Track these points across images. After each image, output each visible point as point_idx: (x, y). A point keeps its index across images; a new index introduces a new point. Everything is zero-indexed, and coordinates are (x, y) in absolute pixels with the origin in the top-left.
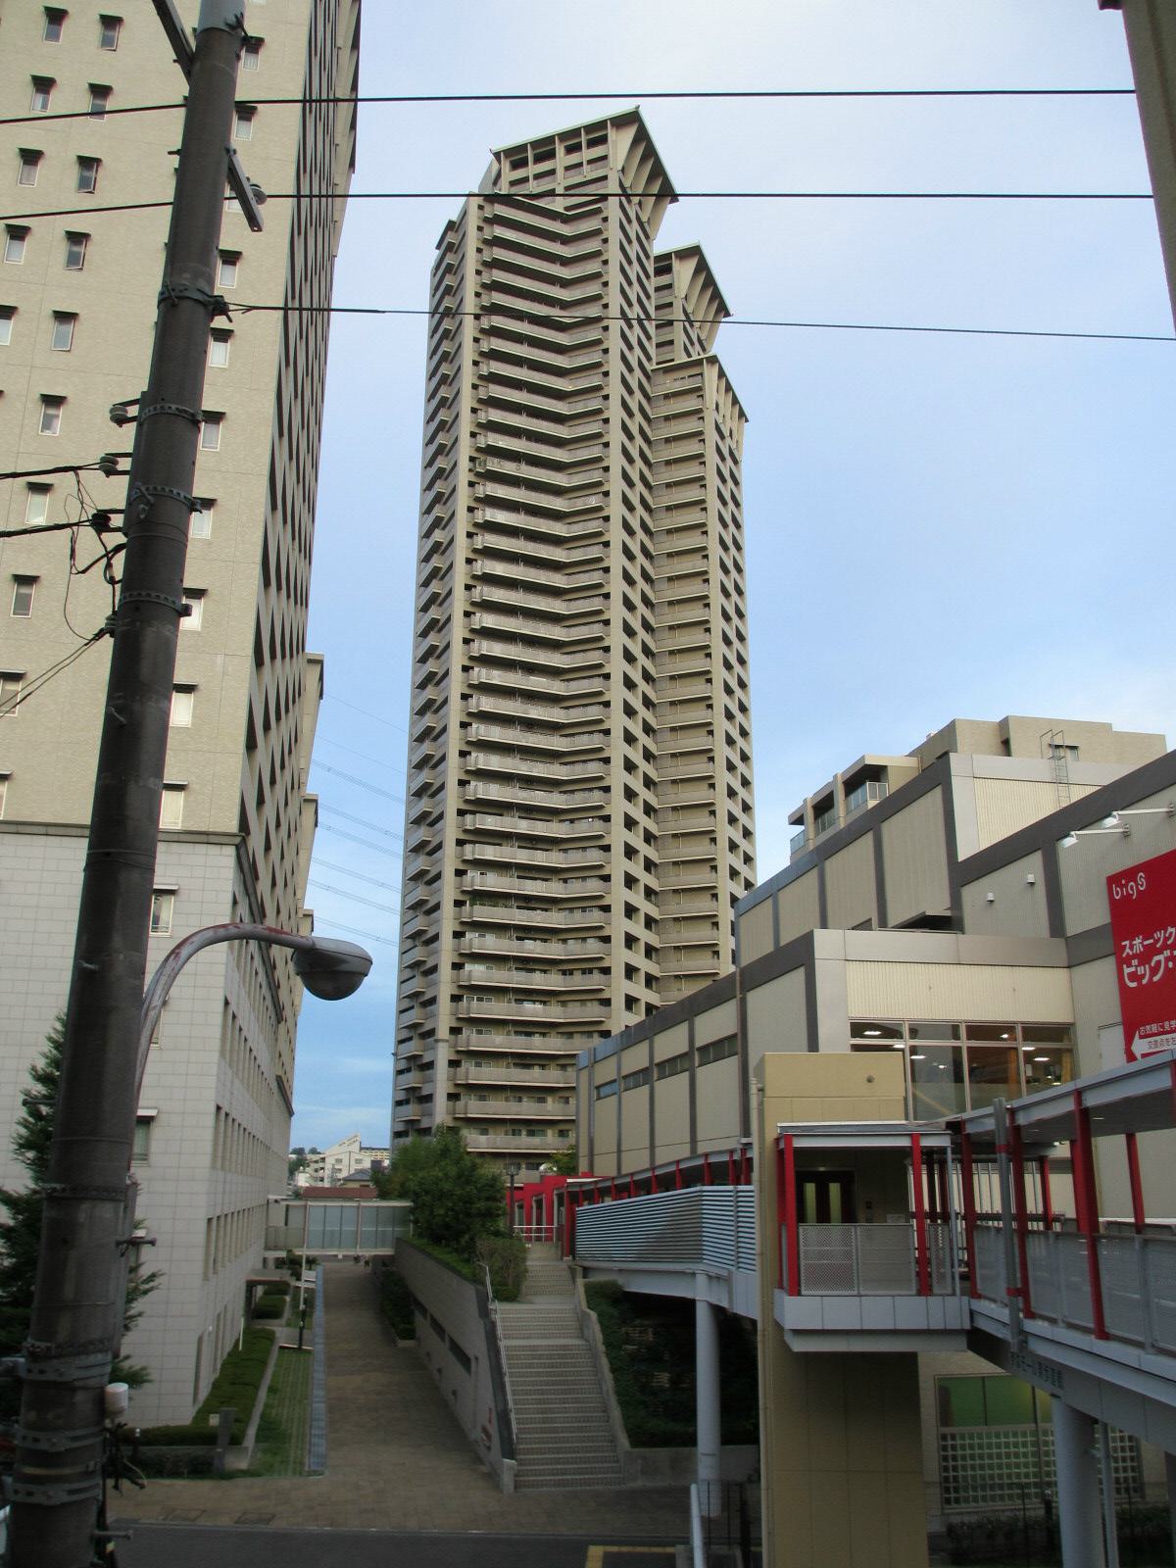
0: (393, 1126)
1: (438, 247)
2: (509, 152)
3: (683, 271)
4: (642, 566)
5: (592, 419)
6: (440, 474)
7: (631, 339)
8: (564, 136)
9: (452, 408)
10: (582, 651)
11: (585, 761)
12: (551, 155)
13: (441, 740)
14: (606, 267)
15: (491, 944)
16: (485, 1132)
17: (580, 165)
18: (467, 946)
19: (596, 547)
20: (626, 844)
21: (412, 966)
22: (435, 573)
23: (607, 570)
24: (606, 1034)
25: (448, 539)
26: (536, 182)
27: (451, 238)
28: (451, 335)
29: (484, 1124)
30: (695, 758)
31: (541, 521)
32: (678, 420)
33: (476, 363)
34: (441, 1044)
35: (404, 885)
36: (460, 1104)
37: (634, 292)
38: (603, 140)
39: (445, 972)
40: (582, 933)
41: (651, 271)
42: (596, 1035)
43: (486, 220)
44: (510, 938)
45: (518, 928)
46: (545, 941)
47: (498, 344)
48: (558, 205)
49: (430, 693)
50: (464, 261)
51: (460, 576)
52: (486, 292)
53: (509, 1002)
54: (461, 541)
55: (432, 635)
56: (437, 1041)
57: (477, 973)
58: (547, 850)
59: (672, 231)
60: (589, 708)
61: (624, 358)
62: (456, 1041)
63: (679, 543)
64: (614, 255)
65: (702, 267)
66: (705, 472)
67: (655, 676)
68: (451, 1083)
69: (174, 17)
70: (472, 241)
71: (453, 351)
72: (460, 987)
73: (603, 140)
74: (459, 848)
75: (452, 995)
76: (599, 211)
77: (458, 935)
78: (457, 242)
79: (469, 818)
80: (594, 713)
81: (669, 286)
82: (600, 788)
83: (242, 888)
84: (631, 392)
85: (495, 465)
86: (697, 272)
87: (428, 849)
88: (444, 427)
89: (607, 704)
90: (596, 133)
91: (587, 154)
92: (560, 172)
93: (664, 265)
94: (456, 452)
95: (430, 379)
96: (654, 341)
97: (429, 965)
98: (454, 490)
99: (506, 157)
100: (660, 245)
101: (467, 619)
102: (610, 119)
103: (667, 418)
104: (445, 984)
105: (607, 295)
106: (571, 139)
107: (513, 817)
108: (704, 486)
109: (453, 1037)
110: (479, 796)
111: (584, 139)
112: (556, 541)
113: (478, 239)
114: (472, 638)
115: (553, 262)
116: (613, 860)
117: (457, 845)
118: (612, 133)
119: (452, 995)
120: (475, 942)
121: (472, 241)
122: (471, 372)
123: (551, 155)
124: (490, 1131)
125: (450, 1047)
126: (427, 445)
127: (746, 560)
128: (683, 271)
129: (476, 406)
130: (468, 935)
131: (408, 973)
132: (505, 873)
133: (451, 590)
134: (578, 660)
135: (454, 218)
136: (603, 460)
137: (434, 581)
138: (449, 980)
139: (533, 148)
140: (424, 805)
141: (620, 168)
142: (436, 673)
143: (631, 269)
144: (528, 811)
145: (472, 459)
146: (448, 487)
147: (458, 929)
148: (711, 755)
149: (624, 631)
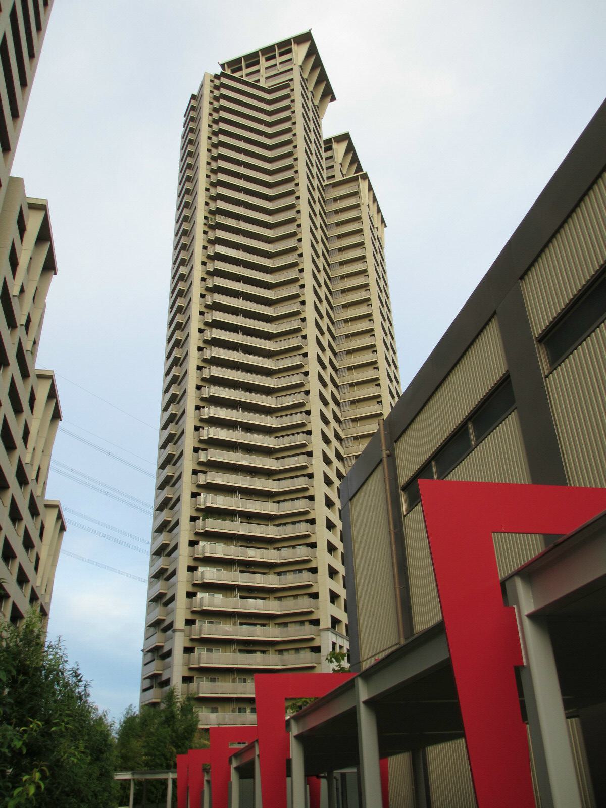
1: (185, 116)
3: (339, 150)
7: (312, 160)
9: (184, 348)
11: (293, 500)
13: (175, 531)
14: (302, 290)
15: (220, 550)
16: (215, 710)
17: (276, 65)
19: (297, 357)
20: (330, 566)
25: (184, 354)
27: (193, 103)
28: (184, 294)
29: (214, 703)
31: (256, 340)
33: (199, 368)
34: (177, 634)
36: (193, 686)
37: (324, 307)
38: (290, 51)
40: (297, 645)
41: (325, 178)
42: (307, 624)
44: (236, 546)
45: (241, 588)
46: (264, 625)
47: (220, 265)
48: (262, 84)
49: (168, 471)
50: (191, 304)
51: (194, 360)
52: (211, 261)
53: (235, 597)
56: (174, 631)
57: (209, 574)
59: (331, 124)
60: (297, 502)
61: (317, 308)
62: (191, 631)
63: (362, 410)
64: (307, 265)
65: (350, 149)
66: (380, 392)
68: (189, 611)
70: (206, 108)
71: (184, 322)
72: (191, 669)
73: (290, 51)
74: (187, 656)
80: (300, 505)
81: (332, 157)
82: (307, 521)
84: (323, 350)
86: (347, 152)
87: (165, 576)
88: (181, 311)
89: (311, 498)
90: (285, 47)
91: (279, 59)
93: (328, 145)
97: (166, 650)
98: (184, 412)
100: (327, 134)
101: (197, 432)
102: (293, 38)
103: (347, 336)
106: (269, 52)
107: (235, 571)
108: (379, 385)
110: (206, 554)
111: (277, 52)
112: (268, 372)
114: (193, 646)
115: (261, 124)
117: (200, 314)
118: (294, 47)
120: (207, 548)
121: (206, 108)
122: (194, 395)
123: (257, 63)
124: (219, 709)
125: (185, 636)
127: (400, 374)
128: (339, 150)
130: (200, 595)
134: (286, 421)
135: (196, 93)
136: (304, 385)
138: (185, 607)
139: (246, 61)
140: (162, 539)
142: (168, 545)
143: (317, 232)
144: (249, 517)
145: (206, 218)
149: (324, 460)
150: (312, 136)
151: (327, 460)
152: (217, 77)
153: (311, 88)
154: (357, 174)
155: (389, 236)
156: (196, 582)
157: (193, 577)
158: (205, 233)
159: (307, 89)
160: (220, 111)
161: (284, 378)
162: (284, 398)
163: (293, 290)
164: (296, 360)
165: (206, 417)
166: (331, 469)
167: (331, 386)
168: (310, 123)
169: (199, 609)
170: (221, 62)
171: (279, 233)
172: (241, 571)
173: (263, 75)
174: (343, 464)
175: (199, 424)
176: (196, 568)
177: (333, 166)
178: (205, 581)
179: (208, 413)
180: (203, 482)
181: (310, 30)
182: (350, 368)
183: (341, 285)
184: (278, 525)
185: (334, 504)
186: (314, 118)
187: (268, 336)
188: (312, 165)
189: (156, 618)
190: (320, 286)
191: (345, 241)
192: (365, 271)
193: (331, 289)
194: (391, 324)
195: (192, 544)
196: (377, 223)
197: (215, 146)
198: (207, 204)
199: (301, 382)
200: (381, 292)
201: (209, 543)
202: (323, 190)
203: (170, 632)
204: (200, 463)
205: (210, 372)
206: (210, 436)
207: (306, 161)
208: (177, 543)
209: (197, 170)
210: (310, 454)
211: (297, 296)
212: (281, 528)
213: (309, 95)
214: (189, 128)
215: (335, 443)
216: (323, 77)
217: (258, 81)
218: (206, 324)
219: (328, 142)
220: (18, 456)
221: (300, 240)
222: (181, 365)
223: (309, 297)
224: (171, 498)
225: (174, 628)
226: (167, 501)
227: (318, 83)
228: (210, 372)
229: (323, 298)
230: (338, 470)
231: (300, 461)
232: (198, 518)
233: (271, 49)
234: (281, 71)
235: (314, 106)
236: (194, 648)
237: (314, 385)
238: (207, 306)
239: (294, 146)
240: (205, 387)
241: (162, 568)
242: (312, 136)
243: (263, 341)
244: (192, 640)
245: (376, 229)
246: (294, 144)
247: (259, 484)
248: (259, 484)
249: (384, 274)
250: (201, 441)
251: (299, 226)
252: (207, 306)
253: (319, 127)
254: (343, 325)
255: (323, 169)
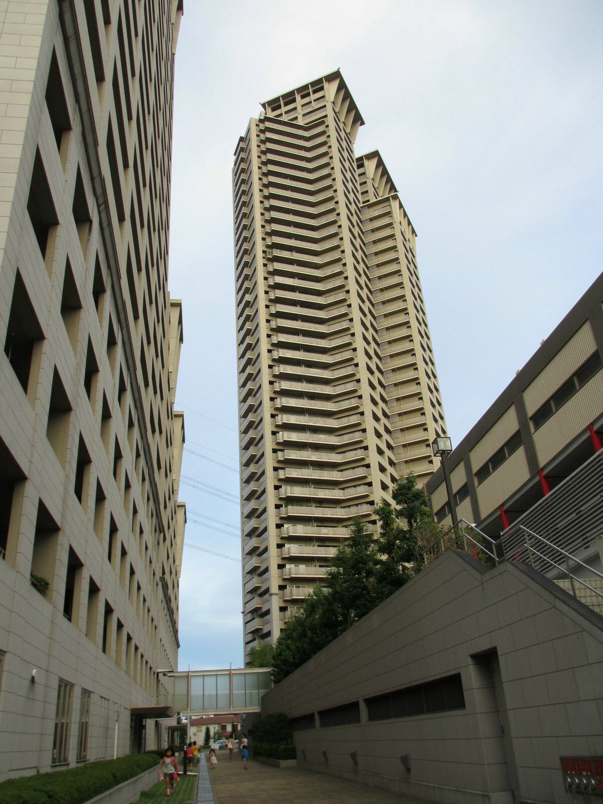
0: (245, 660)
1: (235, 155)
2: (270, 103)
3: (370, 166)
4: (380, 393)
5: (340, 335)
6: (249, 347)
8: (300, 90)
10: (347, 416)
11: (355, 486)
12: (294, 101)
13: (263, 517)
15: (300, 530)
17: (311, 102)
18: (287, 574)
19: (350, 367)
21: (252, 612)
22: (250, 409)
23: (366, 448)
24: (372, 503)
26: (286, 115)
27: (242, 145)
30: (413, 415)
32: (392, 316)
35: (243, 559)
37: (359, 255)
38: (322, 89)
39: (274, 571)
41: (355, 167)
43: (266, 209)
47: (283, 338)
48: (301, 122)
49: (252, 468)
51: (267, 409)
52: (268, 224)
53: (315, 566)
54: (266, 387)
55: (251, 431)
56: (271, 595)
57: (294, 549)
58: (335, 508)
60: (356, 470)
61: (357, 282)
65: (380, 163)
67: (396, 462)
68: (280, 579)
69: (66, 56)
70: (254, 141)
73: (322, 89)
74: (282, 613)
75: (279, 585)
76: (323, 122)
77: (281, 567)
78: (248, 224)
79: (281, 472)
80: (360, 472)
81: (364, 174)
83: (140, 436)
84: (365, 315)
85: (277, 253)
86: (378, 166)
87: (258, 552)
89: (368, 466)
90: (318, 86)
91: (313, 97)
92: (299, 108)
93: (360, 163)
94: (259, 347)
95: (239, 318)
96: (359, 183)
98: (260, 387)
99: (269, 106)
100: (357, 154)
101: (274, 436)
103: (386, 316)
104: (273, 558)
105: (332, 152)
106: (304, 91)
109: (281, 591)
111: (311, 90)
113: (258, 141)
114: (284, 563)
116: (375, 491)
117: (271, 417)
119: (279, 585)
120: (291, 529)
121: (254, 141)
122: (261, 231)
123: (294, 101)
126: (239, 345)
127: (435, 356)
128: (370, 166)
129: (270, 333)
130: (288, 566)
131: (250, 637)
132: (309, 544)
133: (258, 339)
134: (345, 422)
135: (243, 135)
136: (345, 286)
137: (251, 430)
139: (283, 99)
140: (253, 523)
141: (332, 100)
144: (317, 447)
145: (264, 252)
146: (253, 325)
147: (279, 522)
148: (420, 396)
150: (345, 154)
151: (380, 452)
152: (261, 121)
153: (342, 119)
154: (389, 195)
155: (420, 245)
156: (284, 556)
157: (282, 574)
158: (265, 265)
159: (339, 121)
160: (266, 122)
161: (340, 386)
162: (341, 403)
163: (336, 255)
164: (343, 310)
165: (280, 423)
166: (380, 425)
167: (375, 359)
168: (344, 153)
169: (288, 577)
170: (262, 102)
171: (328, 272)
172: (318, 546)
173: (301, 114)
174: (393, 453)
175: (273, 396)
176: (282, 525)
177: (365, 183)
178: (291, 555)
179: (279, 370)
180: (283, 477)
181: (338, 69)
182: (392, 356)
183: (386, 323)
184: (344, 507)
185: (389, 487)
186: (350, 158)
187: (321, 321)
188: (341, 130)
189: (255, 607)
190: (357, 250)
191: (386, 282)
192: (393, 235)
193: (377, 327)
194: (420, 290)
195: (279, 526)
196: (408, 235)
197: (263, 142)
198: (260, 179)
199: (357, 405)
200: (410, 263)
201: (291, 525)
202: (360, 211)
203: (267, 596)
204: (279, 462)
205: (280, 386)
206: (286, 439)
207: (339, 149)
208: (264, 470)
209: (249, 152)
210: (357, 365)
211: (341, 273)
212: (346, 509)
213: (341, 126)
214: (241, 190)
215: (381, 404)
216: (353, 107)
217: (296, 118)
218: (271, 300)
219: (360, 159)
220: (126, 633)
221: (338, 214)
222: (250, 280)
223: (349, 260)
224: (255, 438)
225: (270, 592)
226: (251, 424)
227: (349, 111)
228: (280, 386)
229: (358, 248)
230: (389, 458)
231: (360, 472)
232: (281, 506)
233: (306, 87)
234: (315, 108)
235: (346, 134)
236: (286, 586)
237: (361, 359)
238: (270, 286)
239: (328, 147)
240: (272, 320)
241: (255, 546)
242: (345, 154)
243: (315, 297)
244: (285, 601)
245: (408, 242)
246: (339, 224)
247: (326, 475)
248: (326, 475)
249: (415, 270)
250: (278, 444)
251: (334, 180)
252: (269, 273)
253: (352, 152)
254: (376, 269)
255: (353, 161)
